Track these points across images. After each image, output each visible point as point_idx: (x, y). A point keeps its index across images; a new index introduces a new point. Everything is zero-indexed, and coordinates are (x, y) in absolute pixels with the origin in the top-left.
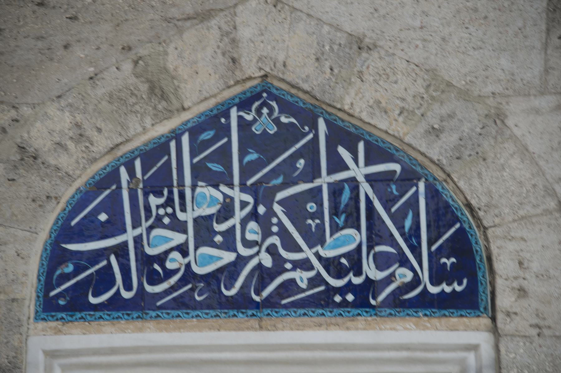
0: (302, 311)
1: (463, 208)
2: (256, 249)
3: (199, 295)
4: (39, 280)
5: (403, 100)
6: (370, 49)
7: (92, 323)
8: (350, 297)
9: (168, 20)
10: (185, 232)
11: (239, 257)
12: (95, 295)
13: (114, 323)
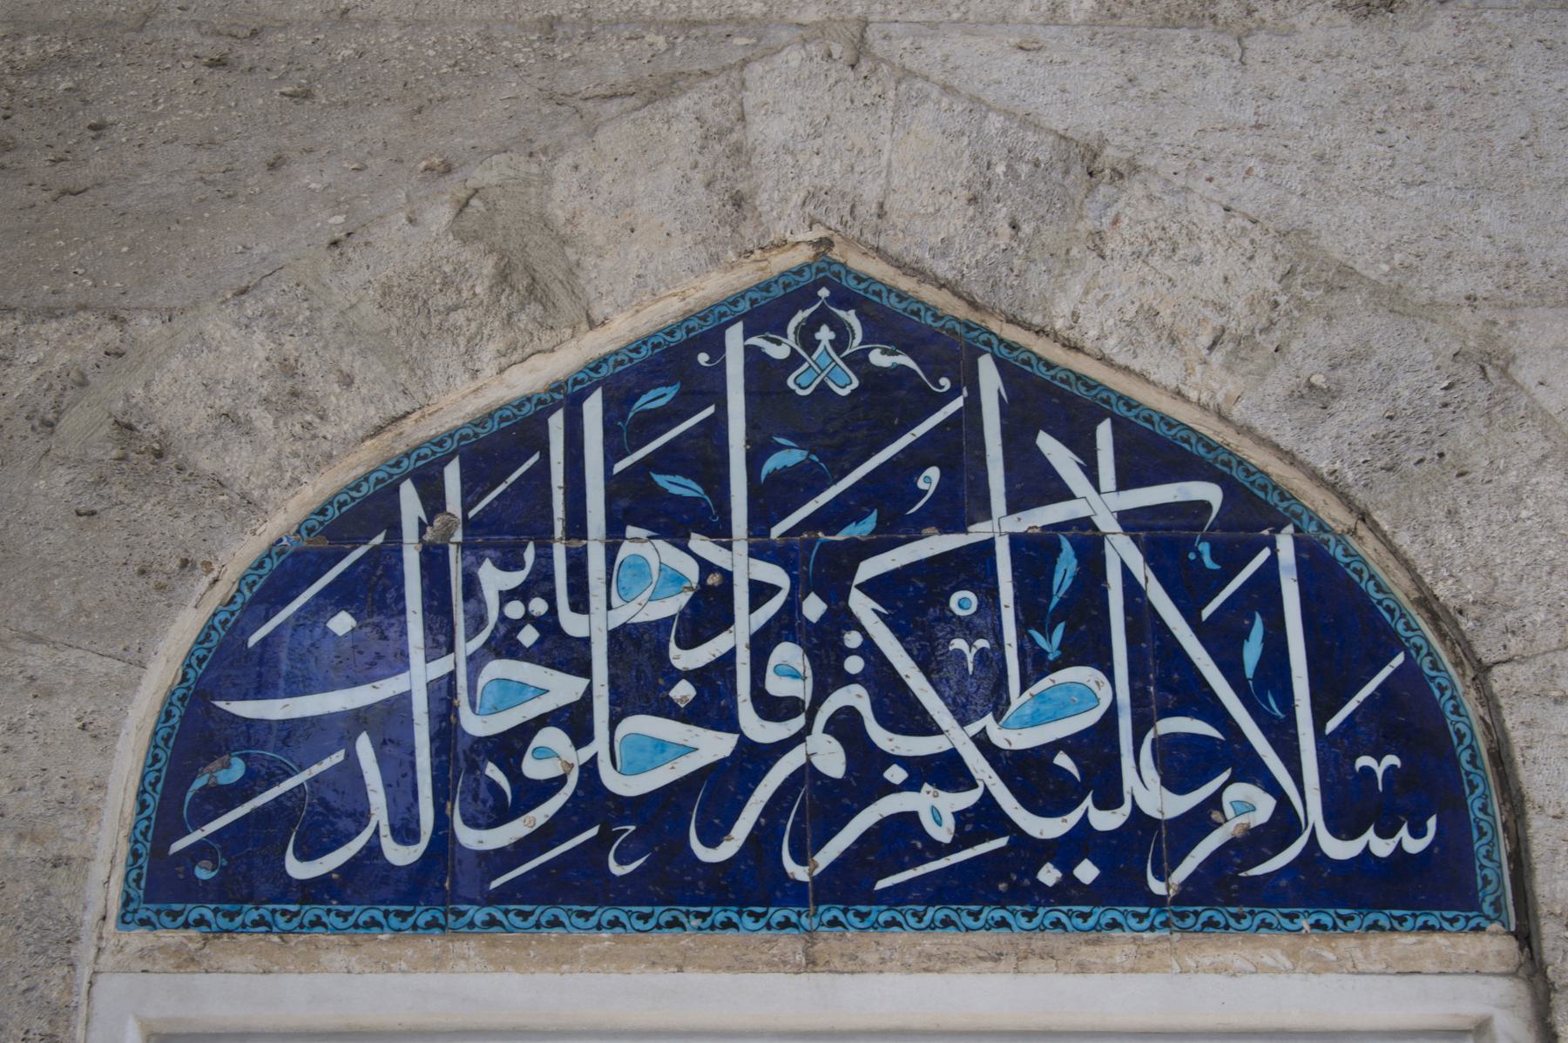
0: (935, 913)
1: (1412, 610)
2: (798, 723)
3: (621, 861)
4: (143, 806)
5: (1222, 308)
6: (1121, 176)
7: (293, 939)
8: (1087, 872)
9: (556, 99)
10: (582, 668)
11: (745, 743)
12: (304, 855)
13: (358, 938)
